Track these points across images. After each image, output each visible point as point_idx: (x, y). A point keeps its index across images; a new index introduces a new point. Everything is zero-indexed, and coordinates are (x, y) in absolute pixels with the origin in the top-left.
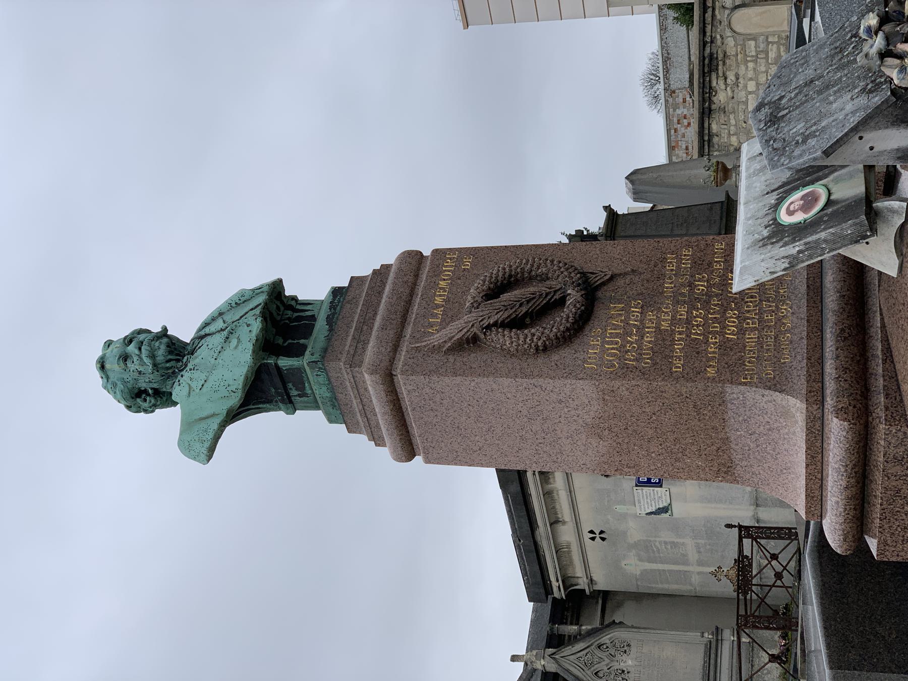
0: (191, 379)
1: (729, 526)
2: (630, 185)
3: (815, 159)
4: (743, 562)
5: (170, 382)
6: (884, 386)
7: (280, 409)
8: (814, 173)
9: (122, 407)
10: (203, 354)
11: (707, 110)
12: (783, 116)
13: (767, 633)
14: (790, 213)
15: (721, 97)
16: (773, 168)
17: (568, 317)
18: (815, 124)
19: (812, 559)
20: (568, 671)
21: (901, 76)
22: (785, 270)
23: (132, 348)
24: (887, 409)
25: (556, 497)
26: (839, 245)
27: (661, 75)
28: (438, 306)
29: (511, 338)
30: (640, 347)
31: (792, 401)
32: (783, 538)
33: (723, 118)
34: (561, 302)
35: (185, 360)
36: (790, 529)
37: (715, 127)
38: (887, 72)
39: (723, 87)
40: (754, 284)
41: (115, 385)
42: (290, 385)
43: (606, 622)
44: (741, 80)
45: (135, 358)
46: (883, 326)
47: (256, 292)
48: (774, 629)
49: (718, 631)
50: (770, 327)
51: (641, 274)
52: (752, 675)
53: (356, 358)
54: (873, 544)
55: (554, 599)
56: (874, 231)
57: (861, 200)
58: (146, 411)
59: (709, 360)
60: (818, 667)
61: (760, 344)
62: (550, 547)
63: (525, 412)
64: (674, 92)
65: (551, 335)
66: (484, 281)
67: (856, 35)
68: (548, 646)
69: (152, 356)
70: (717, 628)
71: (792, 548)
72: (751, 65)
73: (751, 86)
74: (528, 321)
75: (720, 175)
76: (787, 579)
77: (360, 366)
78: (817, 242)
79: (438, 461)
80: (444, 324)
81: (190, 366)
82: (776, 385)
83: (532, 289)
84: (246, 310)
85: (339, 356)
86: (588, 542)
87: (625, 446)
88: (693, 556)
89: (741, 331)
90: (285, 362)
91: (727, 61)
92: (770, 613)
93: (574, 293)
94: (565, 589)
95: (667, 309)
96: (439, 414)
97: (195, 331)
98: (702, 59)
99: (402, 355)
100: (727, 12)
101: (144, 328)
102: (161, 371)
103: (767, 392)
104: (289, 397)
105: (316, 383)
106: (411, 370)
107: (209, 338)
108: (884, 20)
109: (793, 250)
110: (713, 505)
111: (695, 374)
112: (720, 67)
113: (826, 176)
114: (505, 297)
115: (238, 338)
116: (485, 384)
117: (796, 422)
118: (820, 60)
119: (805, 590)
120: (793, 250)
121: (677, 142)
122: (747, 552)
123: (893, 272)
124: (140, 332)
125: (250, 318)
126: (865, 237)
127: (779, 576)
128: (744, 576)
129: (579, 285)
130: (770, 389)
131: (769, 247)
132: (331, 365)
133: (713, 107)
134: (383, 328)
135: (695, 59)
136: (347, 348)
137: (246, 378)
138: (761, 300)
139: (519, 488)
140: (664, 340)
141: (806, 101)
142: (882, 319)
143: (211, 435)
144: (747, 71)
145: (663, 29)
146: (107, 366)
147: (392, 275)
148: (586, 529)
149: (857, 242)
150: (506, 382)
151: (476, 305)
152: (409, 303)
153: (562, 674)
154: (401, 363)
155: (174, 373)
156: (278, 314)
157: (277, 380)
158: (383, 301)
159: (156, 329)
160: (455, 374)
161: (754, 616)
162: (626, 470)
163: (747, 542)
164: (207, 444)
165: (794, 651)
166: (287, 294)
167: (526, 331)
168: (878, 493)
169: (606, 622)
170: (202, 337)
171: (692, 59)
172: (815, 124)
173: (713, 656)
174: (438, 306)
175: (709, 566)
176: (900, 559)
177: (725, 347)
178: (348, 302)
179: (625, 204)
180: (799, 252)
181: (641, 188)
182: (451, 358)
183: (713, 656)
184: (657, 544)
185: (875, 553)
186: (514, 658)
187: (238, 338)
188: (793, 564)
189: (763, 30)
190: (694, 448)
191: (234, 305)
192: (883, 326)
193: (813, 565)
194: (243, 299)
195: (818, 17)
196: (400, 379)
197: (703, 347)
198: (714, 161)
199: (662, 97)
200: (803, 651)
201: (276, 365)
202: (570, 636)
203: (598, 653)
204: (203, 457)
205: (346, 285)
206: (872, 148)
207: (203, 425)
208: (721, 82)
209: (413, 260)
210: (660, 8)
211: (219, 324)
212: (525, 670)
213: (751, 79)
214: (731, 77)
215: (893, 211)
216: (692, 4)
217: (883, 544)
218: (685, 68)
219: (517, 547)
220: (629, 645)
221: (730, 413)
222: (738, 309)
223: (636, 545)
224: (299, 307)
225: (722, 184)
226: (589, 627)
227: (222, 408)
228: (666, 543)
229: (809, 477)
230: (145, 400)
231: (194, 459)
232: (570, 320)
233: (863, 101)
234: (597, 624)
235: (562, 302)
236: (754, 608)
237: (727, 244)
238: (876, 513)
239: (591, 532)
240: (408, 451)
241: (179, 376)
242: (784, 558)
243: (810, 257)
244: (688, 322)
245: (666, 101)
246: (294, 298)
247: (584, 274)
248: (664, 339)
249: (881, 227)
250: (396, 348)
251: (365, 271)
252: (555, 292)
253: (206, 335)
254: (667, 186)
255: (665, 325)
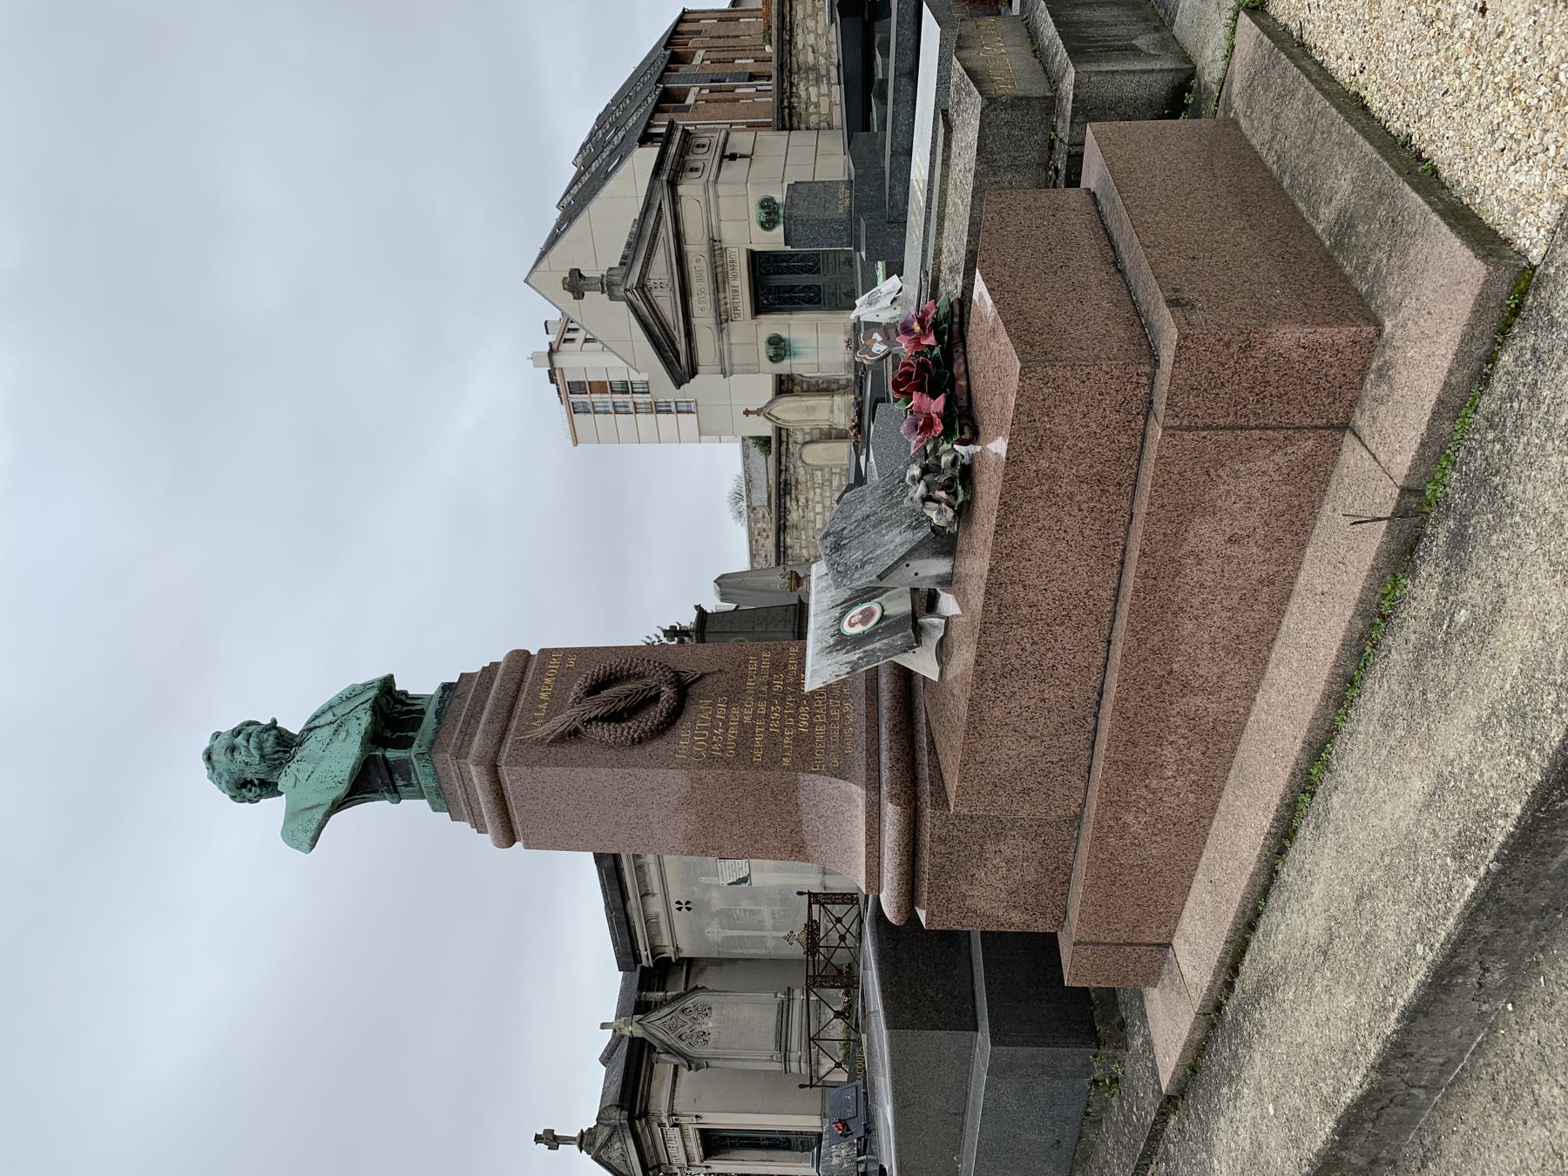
0: (298, 770)
1: (800, 893)
2: (718, 588)
3: (871, 582)
4: (812, 926)
5: (276, 773)
6: (930, 775)
7: (385, 799)
8: (869, 592)
9: (227, 797)
10: (312, 745)
11: (782, 527)
12: (845, 545)
13: (832, 991)
14: (852, 625)
15: (794, 516)
16: (837, 588)
17: (662, 712)
18: (871, 552)
19: (872, 927)
20: (654, 1035)
21: (939, 517)
22: (847, 673)
23: (240, 740)
24: (932, 794)
25: (647, 871)
26: (891, 654)
27: (744, 494)
28: (542, 701)
29: (609, 731)
30: (725, 739)
31: (854, 787)
32: (846, 903)
33: (795, 534)
34: (656, 699)
35: (292, 752)
36: (852, 894)
37: (789, 540)
38: (928, 513)
39: (795, 508)
40: (822, 685)
41: (220, 775)
42: (397, 776)
43: (690, 988)
44: (810, 503)
45: (243, 750)
46: (928, 722)
47: (367, 687)
48: (839, 987)
49: (789, 991)
50: (835, 722)
51: (726, 673)
52: (820, 1031)
53: (463, 750)
54: (922, 914)
55: (643, 968)
56: (919, 642)
57: (908, 616)
58: (250, 801)
59: (785, 750)
60: (877, 1027)
61: (827, 735)
62: (640, 918)
63: (620, 800)
64: (755, 509)
65: (646, 729)
66: (586, 678)
67: (903, 481)
68: (636, 1013)
69: (260, 748)
70: (789, 988)
71: (854, 912)
72: (818, 491)
73: (819, 508)
74: (626, 715)
75: (794, 582)
76: (850, 941)
77: (466, 758)
78: (873, 650)
79: (538, 846)
80: (547, 719)
81: (297, 757)
82: (841, 773)
83: (630, 686)
84: (357, 704)
85: (446, 748)
86: (675, 912)
87: (710, 830)
88: (769, 922)
89: (812, 725)
90: (392, 754)
91: (799, 487)
92: (835, 973)
93: (668, 690)
94: (653, 958)
95: (749, 703)
96: (540, 802)
97: (305, 722)
98: (778, 484)
99: (507, 747)
100: (799, 446)
101: (253, 720)
102: (268, 762)
103: (833, 780)
104: (395, 787)
105: (422, 774)
106: (514, 761)
107: (317, 731)
108: (925, 471)
109: (854, 656)
110: (787, 874)
111: (772, 763)
112: (793, 492)
113: (880, 595)
114: (604, 693)
115: (347, 731)
116: (584, 773)
117: (858, 806)
118: (874, 499)
119: (864, 956)
120: (854, 656)
121: (758, 551)
122: (815, 917)
123: (935, 678)
124: (250, 723)
125: (360, 713)
126: (913, 647)
127: (842, 938)
128: (813, 939)
129: (672, 683)
130: (836, 777)
131: (835, 654)
132: (438, 757)
133: (788, 524)
134: (490, 721)
135: (772, 482)
136: (454, 741)
137: (354, 769)
138: (828, 698)
139: (613, 863)
140: (746, 733)
141: (864, 533)
142: (927, 716)
143: (315, 825)
144: (815, 495)
145: (746, 456)
146: (214, 757)
147: (500, 671)
148: (673, 901)
149: (905, 651)
150: (604, 771)
151: (579, 700)
152: (516, 698)
153: (648, 1039)
154: (505, 755)
155: (281, 764)
156: (388, 708)
157: (383, 771)
158: (491, 696)
159: (266, 721)
160: (557, 765)
161: (822, 977)
162: (711, 851)
163: (815, 907)
164: (310, 834)
165: (855, 1007)
166: (398, 688)
167: (623, 725)
168: (926, 869)
169: (690, 988)
170: (310, 730)
171: (770, 482)
172: (871, 552)
173: (785, 1015)
174: (542, 701)
175: (782, 931)
176: (945, 928)
177: (798, 739)
178: (457, 697)
179: (713, 604)
180: (859, 658)
181: (727, 590)
182: (553, 750)
183: (785, 1015)
184: (737, 912)
185: (924, 924)
186: (604, 1026)
187: (347, 731)
188: (855, 926)
189: (827, 463)
190: (771, 830)
191: (344, 699)
192: (928, 722)
193: (872, 933)
194: (354, 693)
195: (872, 459)
196: (504, 770)
197: (780, 739)
198: (788, 570)
199: (745, 512)
200: (863, 1007)
201: (384, 757)
202: (656, 1002)
203: (682, 1017)
204: (306, 846)
205: (456, 681)
206: (916, 574)
207: (308, 815)
208: (794, 503)
209: (521, 659)
210: (744, 439)
211: (329, 717)
212: (613, 1036)
213: (818, 502)
214: (802, 500)
215: (934, 626)
216: (770, 438)
217: (930, 915)
218: (765, 489)
219: (609, 919)
220: (710, 1008)
221: (803, 799)
222: (809, 705)
223: (719, 913)
224: (408, 701)
225: (795, 590)
226: (674, 993)
227: (328, 798)
228: (745, 910)
229: (868, 854)
230: (250, 790)
231: (297, 848)
232: (664, 714)
233: (909, 535)
234: (681, 990)
235: (656, 698)
236: (821, 969)
237: (800, 649)
238: (924, 888)
239: (678, 903)
240: (509, 836)
241: (286, 768)
242: (847, 921)
243: (868, 663)
244: (767, 716)
245: (749, 516)
246: (404, 693)
247: (677, 673)
248: (746, 731)
249: (924, 639)
250: (501, 740)
251: (475, 668)
252: (651, 689)
253: (316, 727)
254: (749, 590)
255: (747, 719)
